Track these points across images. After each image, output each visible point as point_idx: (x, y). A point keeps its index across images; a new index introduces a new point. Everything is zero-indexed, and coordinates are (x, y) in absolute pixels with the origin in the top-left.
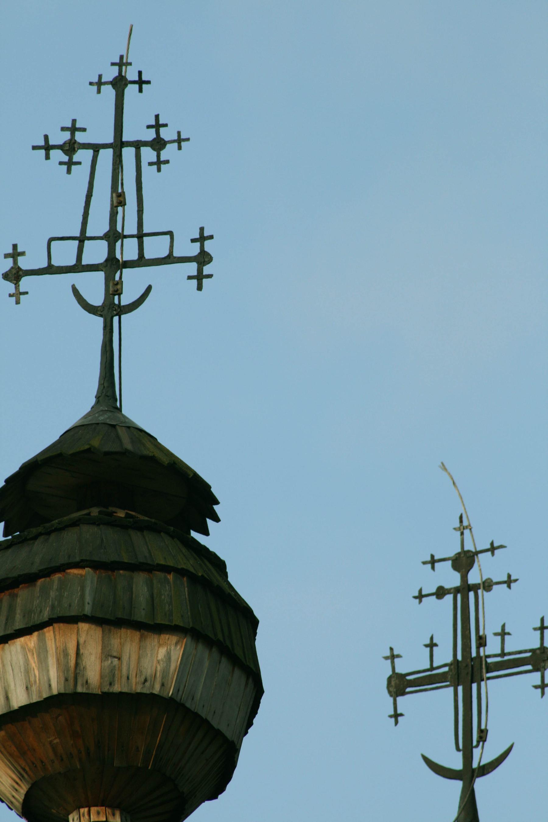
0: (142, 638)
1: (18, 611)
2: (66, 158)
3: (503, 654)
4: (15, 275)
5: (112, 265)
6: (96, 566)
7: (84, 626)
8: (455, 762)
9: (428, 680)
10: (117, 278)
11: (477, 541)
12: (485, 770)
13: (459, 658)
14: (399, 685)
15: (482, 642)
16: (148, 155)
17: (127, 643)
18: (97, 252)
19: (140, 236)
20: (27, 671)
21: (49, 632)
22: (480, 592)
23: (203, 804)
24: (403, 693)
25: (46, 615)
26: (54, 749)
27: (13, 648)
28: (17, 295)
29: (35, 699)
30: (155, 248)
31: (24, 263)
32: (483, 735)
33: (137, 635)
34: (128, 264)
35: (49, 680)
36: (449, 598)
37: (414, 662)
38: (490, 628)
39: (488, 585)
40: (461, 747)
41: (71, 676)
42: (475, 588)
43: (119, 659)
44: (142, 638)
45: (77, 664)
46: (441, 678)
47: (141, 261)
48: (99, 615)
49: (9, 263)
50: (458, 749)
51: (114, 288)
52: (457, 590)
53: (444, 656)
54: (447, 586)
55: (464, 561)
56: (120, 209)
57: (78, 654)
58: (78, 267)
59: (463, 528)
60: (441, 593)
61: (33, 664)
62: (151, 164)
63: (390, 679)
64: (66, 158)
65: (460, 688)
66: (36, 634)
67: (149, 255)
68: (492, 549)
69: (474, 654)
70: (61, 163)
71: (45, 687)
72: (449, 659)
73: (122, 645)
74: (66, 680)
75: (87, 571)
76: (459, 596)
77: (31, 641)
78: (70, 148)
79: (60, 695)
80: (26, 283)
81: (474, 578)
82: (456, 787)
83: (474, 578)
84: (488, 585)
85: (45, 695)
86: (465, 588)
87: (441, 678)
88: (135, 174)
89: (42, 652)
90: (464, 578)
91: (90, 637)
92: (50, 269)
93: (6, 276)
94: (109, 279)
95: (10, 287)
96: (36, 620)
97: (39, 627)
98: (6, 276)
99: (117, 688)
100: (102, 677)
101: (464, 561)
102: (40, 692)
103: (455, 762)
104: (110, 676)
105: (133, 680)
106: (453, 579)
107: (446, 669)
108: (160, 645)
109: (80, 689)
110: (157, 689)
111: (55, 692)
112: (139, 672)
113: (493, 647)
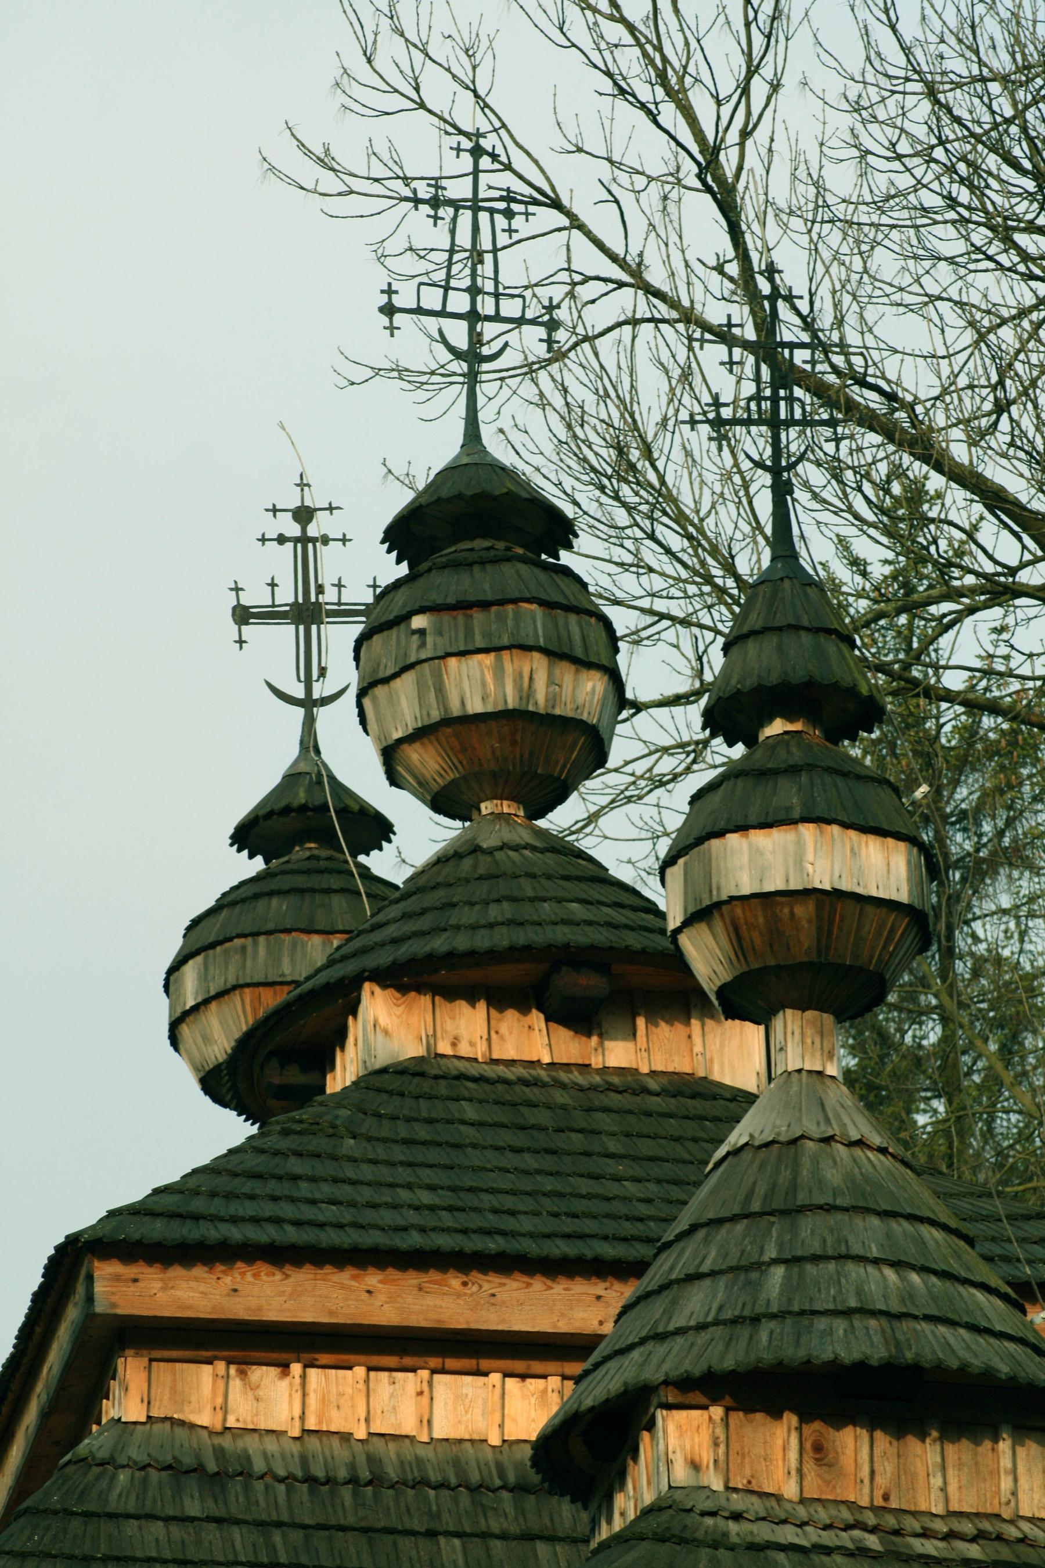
0: (577, 671)
1: (477, 631)
2: (432, 213)
3: (339, 604)
4: (389, 310)
5: (473, 316)
6: (543, 603)
7: (536, 655)
8: (299, 692)
9: (271, 615)
10: (479, 329)
11: (315, 499)
12: (325, 701)
13: (300, 601)
14: (243, 615)
15: (320, 590)
16: (501, 221)
17: (566, 673)
18: (459, 302)
19: (497, 295)
20: (484, 684)
21: (506, 655)
22: (318, 544)
23: (94, 1222)
24: (247, 624)
25: (505, 641)
26: (493, 752)
27: (470, 662)
28: (392, 329)
29: (490, 709)
30: (511, 308)
31: (398, 301)
32: (323, 672)
33: (573, 668)
34: (488, 318)
35: (505, 696)
36: (290, 545)
37: (256, 597)
38: (327, 578)
39: (325, 540)
40: (302, 678)
41: (524, 695)
42: (314, 540)
43: (560, 686)
44: (577, 671)
45: (530, 687)
46: (283, 615)
47: (497, 318)
48: (551, 648)
49: (384, 298)
50: (299, 680)
51: (476, 339)
52: (296, 540)
53: (286, 595)
54: (288, 535)
55: (304, 515)
56: (479, 266)
57: (531, 679)
58: (443, 313)
59: (302, 485)
60: (281, 539)
61: (489, 679)
62: (504, 230)
63: (234, 608)
64: (432, 213)
65: (301, 628)
66: (493, 654)
67: (503, 313)
68: (331, 509)
69: (313, 599)
70: (428, 216)
71: (501, 701)
72: (291, 600)
73: (562, 675)
74: (521, 698)
75: (534, 607)
76: (299, 545)
77: (488, 659)
78: (435, 203)
79: (514, 710)
80: (399, 319)
81: (312, 531)
82: (300, 712)
83: (312, 531)
84: (325, 540)
85: (500, 708)
86: (304, 540)
87: (283, 615)
88: (490, 238)
89: (499, 672)
90: (304, 530)
91: (539, 663)
92: (419, 311)
93: (381, 310)
94: (472, 329)
95: (385, 320)
96: (496, 643)
97: (498, 649)
98: (381, 310)
99: (557, 711)
100: (547, 700)
101: (304, 515)
102: (495, 704)
103: (299, 692)
104: (553, 699)
105: (569, 706)
106: (294, 530)
107: (287, 608)
108: (588, 680)
109: (531, 708)
110: (585, 717)
111: (510, 706)
112: (574, 699)
113: (330, 596)
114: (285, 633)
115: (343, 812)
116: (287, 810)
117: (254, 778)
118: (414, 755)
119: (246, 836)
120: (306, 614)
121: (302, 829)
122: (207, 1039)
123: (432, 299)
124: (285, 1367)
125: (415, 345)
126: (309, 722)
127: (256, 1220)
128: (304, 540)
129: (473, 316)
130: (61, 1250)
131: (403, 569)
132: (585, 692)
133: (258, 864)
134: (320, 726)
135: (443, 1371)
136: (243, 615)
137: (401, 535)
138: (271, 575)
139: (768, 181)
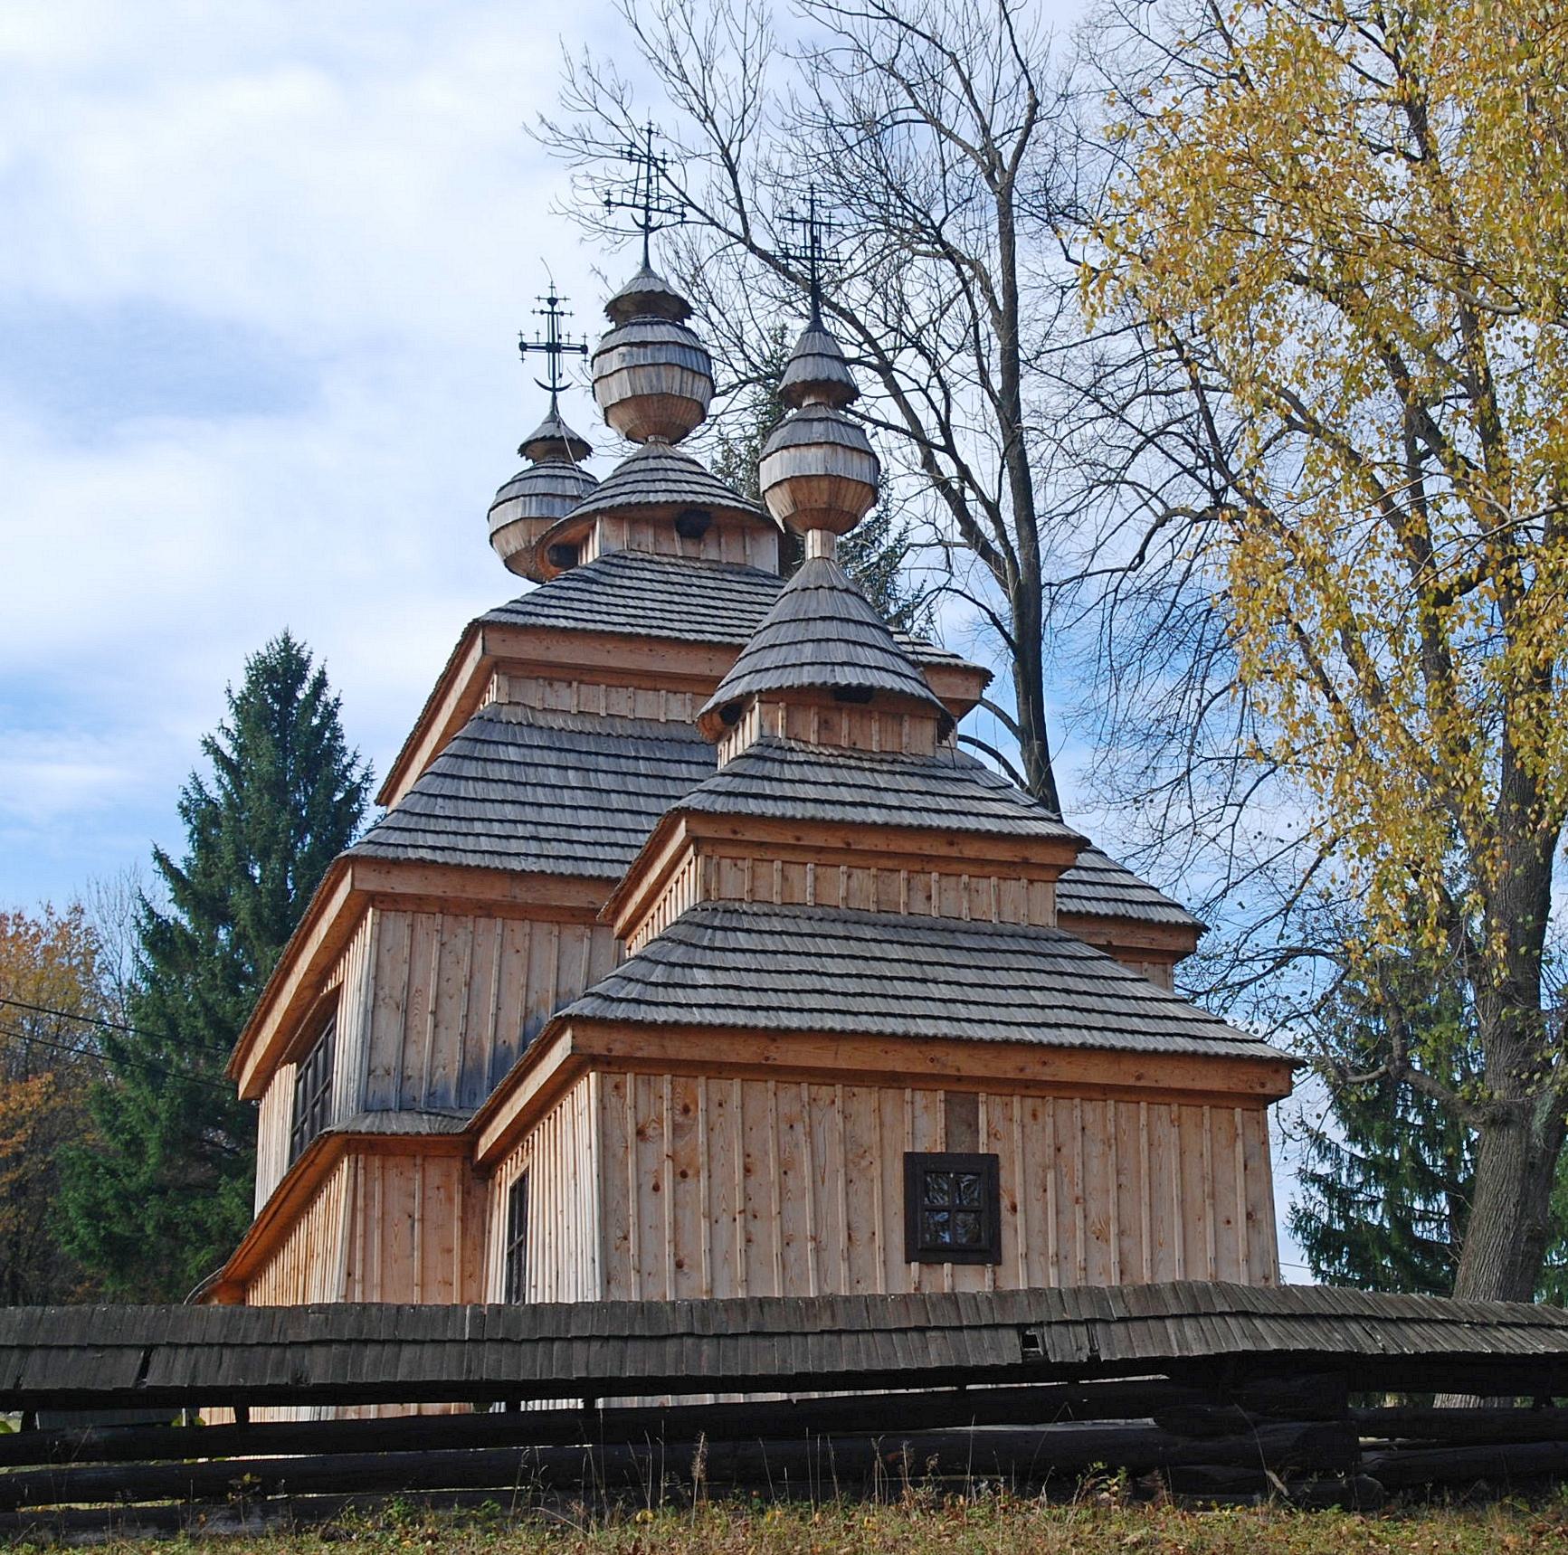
14: (523, 347)
37: (530, 339)
53: (544, 339)
58: (634, 206)
81: (556, 309)
83: (556, 309)
86: (552, 313)
101: (552, 301)
106: (548, 308)
114: (544, 355)
115: (571, 440)
116: (544, 439)
117: (531, 423)
118: (619, 412)
119: (524, 450)
120: (553, 348)
121: (554, 448)
122: (508, 542)
123: (628, 199)
124: (570, 685)
125: (624, 218)
126: (554, 398)
127: (566, 618)
128: (552, 313)
129: (647, 208)
130: (470, 625)
131: (612, 326)
132: (701, 386)
133: (530, 463)
134: (559, 401)
135: (640, 688)
136: (523, 347)
137: (615, 309)
138: (538, 329)
139: (747, 156)
